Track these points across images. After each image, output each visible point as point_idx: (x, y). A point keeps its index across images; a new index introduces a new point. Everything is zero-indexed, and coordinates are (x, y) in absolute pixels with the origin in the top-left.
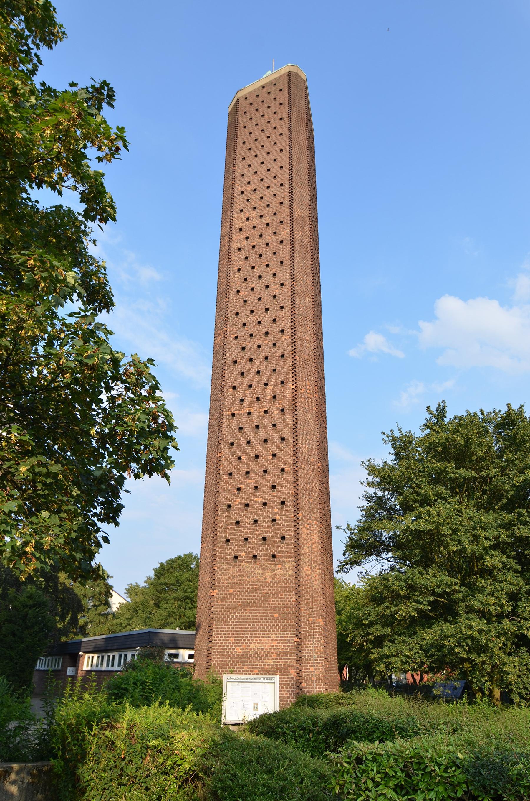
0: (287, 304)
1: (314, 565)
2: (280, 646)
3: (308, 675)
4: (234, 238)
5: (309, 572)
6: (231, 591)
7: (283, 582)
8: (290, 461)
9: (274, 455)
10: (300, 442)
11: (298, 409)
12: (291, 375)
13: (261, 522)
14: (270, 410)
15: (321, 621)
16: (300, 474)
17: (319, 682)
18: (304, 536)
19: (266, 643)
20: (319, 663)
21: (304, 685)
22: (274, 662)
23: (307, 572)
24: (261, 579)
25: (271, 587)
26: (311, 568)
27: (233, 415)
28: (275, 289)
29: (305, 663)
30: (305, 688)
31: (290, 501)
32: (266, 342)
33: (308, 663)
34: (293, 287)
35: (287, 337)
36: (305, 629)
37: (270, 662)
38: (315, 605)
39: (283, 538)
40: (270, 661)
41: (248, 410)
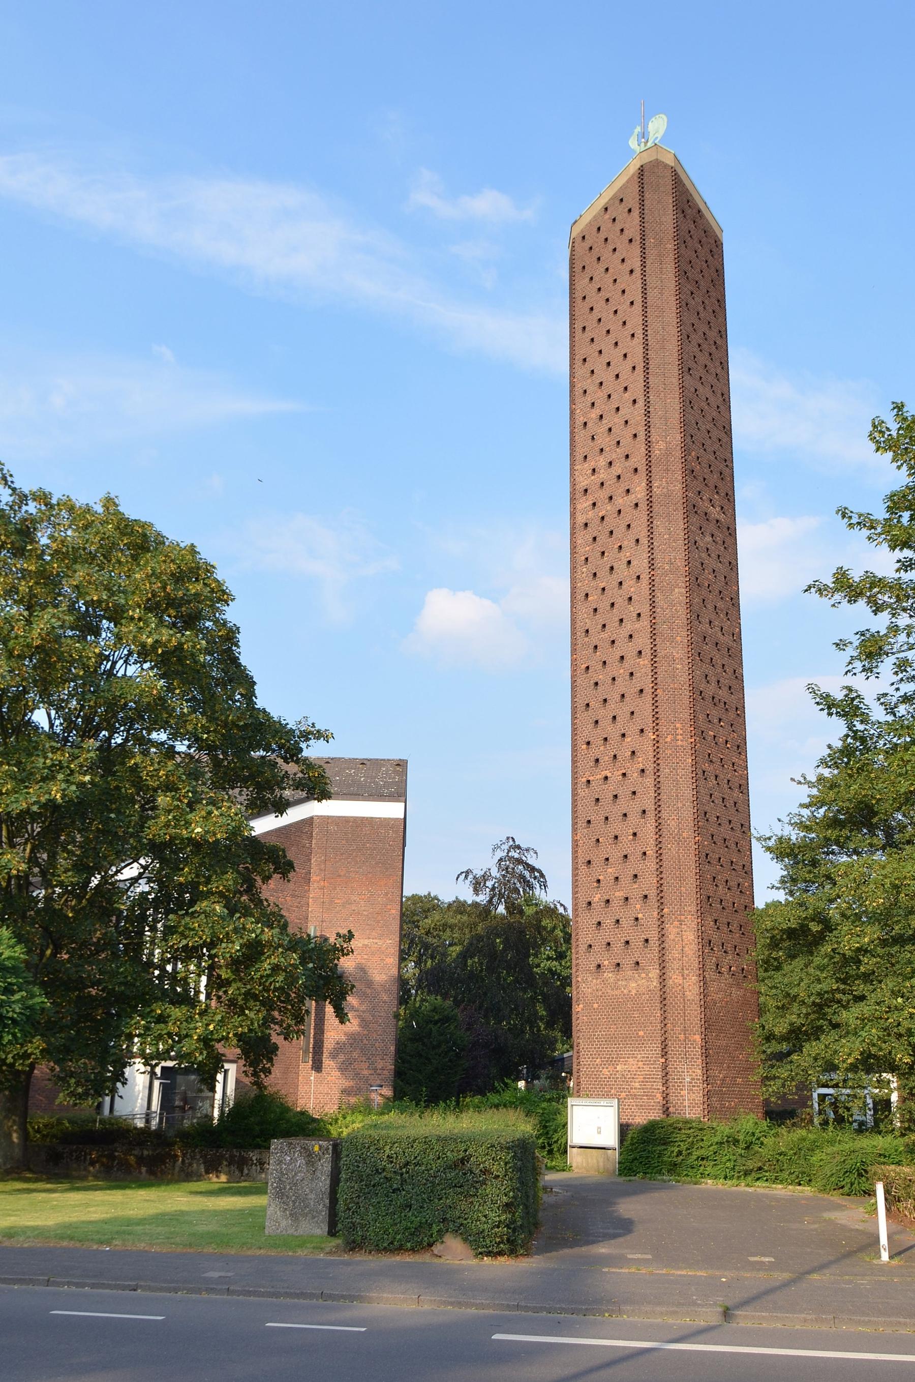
0: (645, 610)
1: (686, 972)
2: (646, 1068)
4: (579, 507)
6: (596, 1006)
8: (652, 842)
9: (635, 834)
10: (664, 814)
11: (661, 767)
12: (651, 719)
13: (623, 922)
14: (629, 772)
15: (698, 1038)
16: (664, 857)
18: (672, 937)
19: (633, 1064)
21: (671, 1109)
24: (625, 991)
27: (588, 781)
28: (630, 587)
30: (674, 1113)
31: (653, 894)
32: (621, 672)
34: (652, 581)
35: (645, 661)
36: (674, 1048)
38: (689, 1020)
39: (647, 941)
41: (605, 773)
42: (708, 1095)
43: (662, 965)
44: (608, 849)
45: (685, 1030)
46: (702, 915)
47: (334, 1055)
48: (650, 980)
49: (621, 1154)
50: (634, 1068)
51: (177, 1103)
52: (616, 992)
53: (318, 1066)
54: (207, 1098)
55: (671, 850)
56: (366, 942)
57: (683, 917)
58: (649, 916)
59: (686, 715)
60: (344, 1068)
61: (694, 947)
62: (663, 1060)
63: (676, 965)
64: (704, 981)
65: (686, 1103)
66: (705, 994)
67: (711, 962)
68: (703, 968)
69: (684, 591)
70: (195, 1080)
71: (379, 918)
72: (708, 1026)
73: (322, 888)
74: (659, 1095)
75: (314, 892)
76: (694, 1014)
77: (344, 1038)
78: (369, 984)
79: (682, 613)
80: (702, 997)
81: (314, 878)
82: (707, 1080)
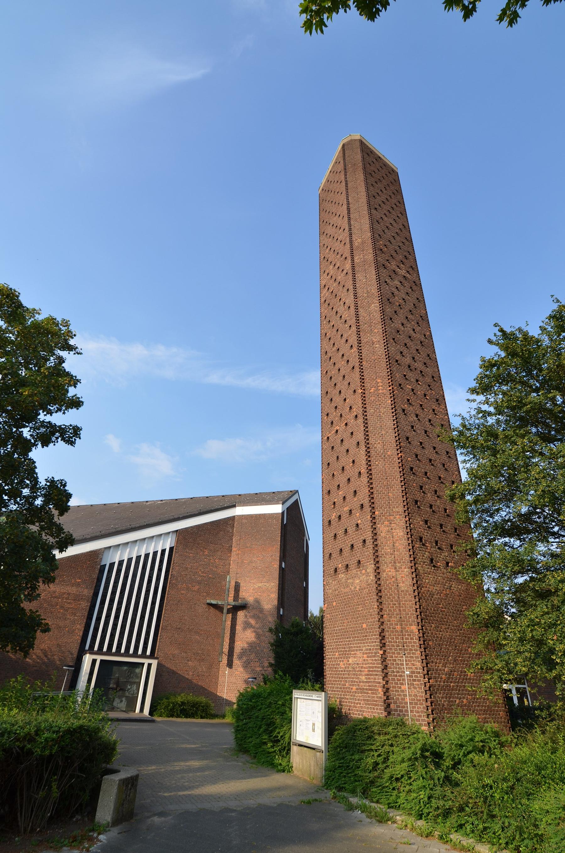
1: (398, 565)
3: (399, 695)
5: (392, 573)
7: (367, 588)
10: (371, 441)
15: (414, 628)
16: (373, 472)
17: (416, 704)
18: (383, 535)
20: (414, 680)
21: (392, 706)
22: (366, 678)
23: (390, 573)
25: (360, 596)
26: (395, 568)
29: (394, 680)
33: (398, 680)
37: (363, 678)
38: (404, 610)
40: (364, 677)
42: (431, 691)
43: (377, 560)
44: (341, 479)
45: (401, 620)
46: (409, 514)
47: (240, 657)
48: (368, 575)
49: (328, 759)
50: (360, 661)
51: (111, 686)
52: (347, 590)
53: (230, 664)
54: (134, 683)
55: (378, 465)
56: (260, 585)
57: (392, 518)
58: (364, 519)
59: (384, 373)
60: (246, 665)
61: (405, 542)
62: (381, 652)
63: (388, 559)
64: (417, 574)
65: (408, 700)
66: (418, 584)
67: (424, 556)
68: (414, 560)
69: (378, 305)
70: (126, 670)
71: (268, 570)
72: (424, 617)
73: (238, 555)
74: (380, 689)
75: (234, 557)
76: (409, 605)
77: (246, 645)
78: (261, 610)
79: (377, 316)
80: (415, 588)
81: (234, 549)
82: (428, 674)
